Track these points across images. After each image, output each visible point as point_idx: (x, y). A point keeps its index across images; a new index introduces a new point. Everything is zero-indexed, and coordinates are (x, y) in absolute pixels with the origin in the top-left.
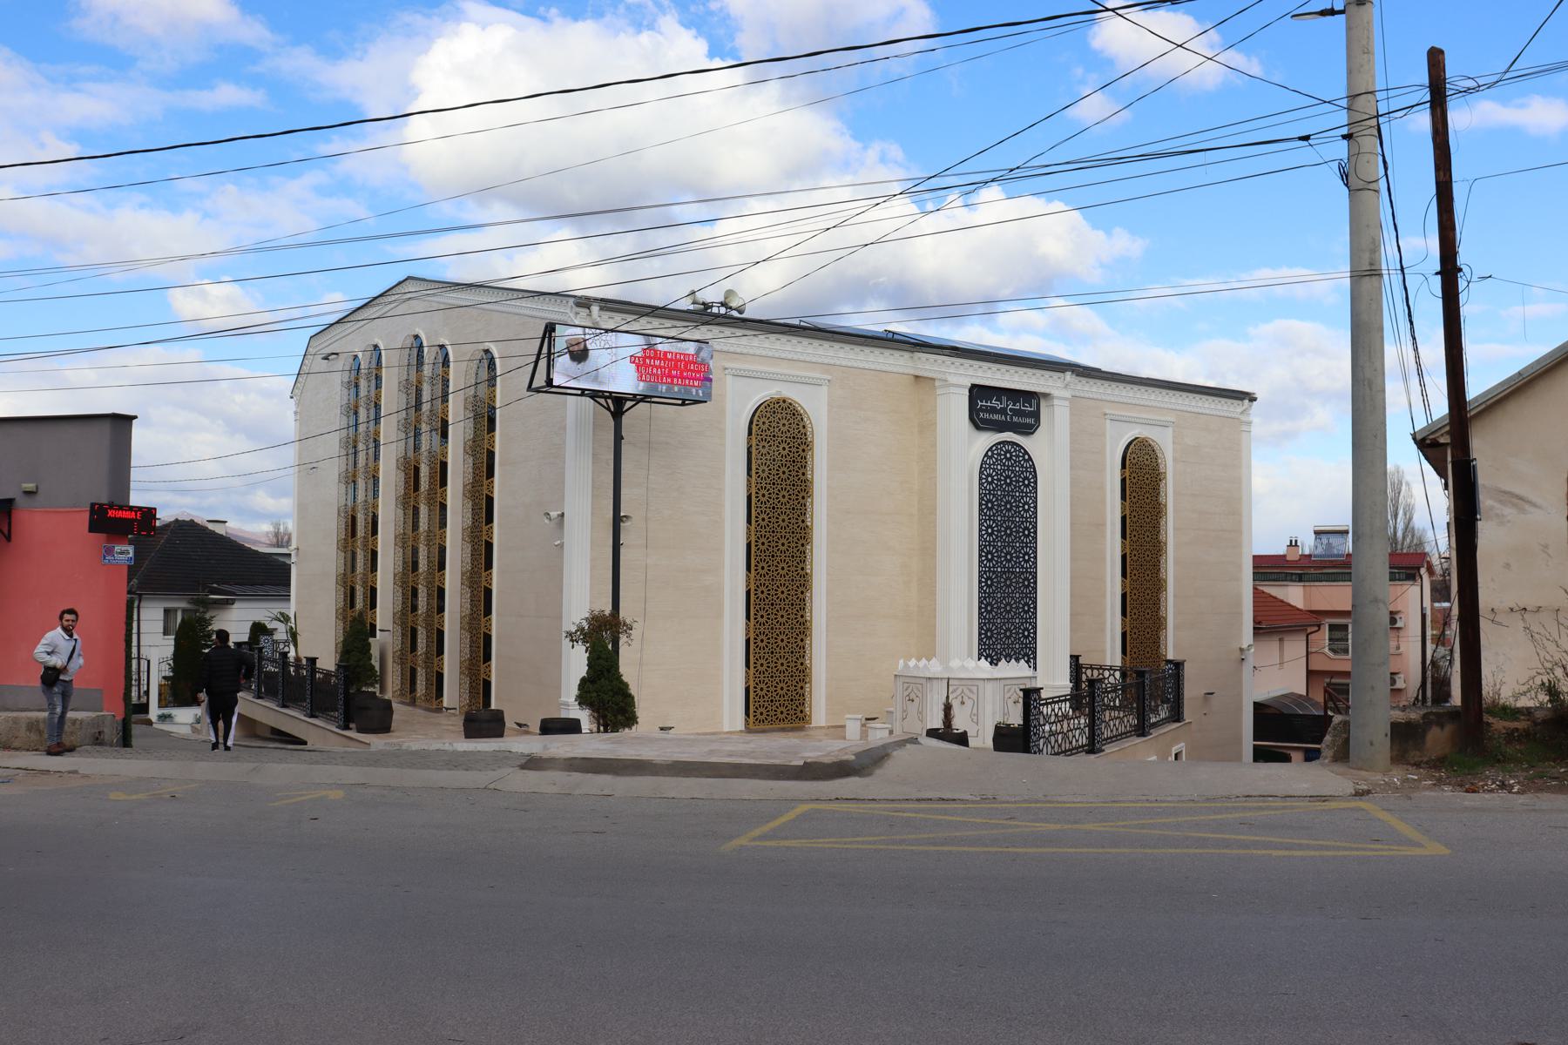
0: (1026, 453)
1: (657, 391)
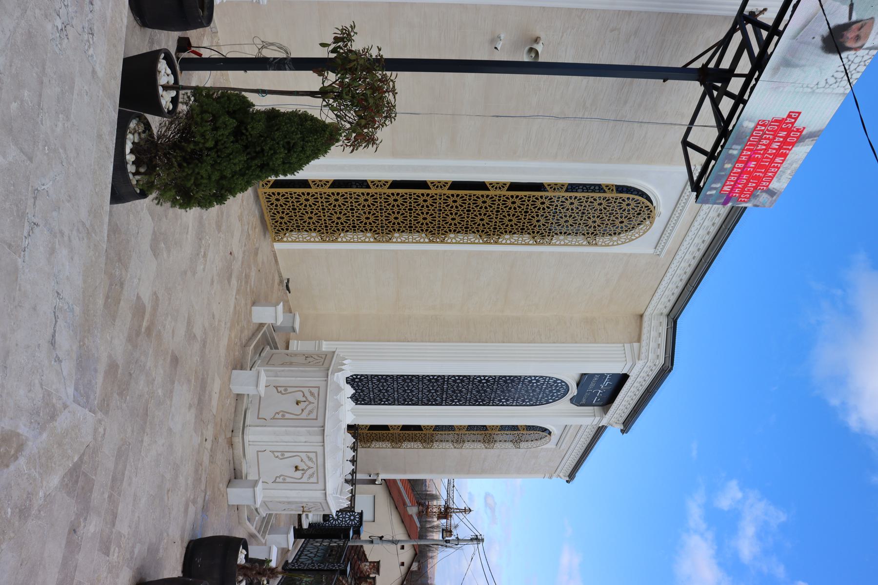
1: (734, 143)
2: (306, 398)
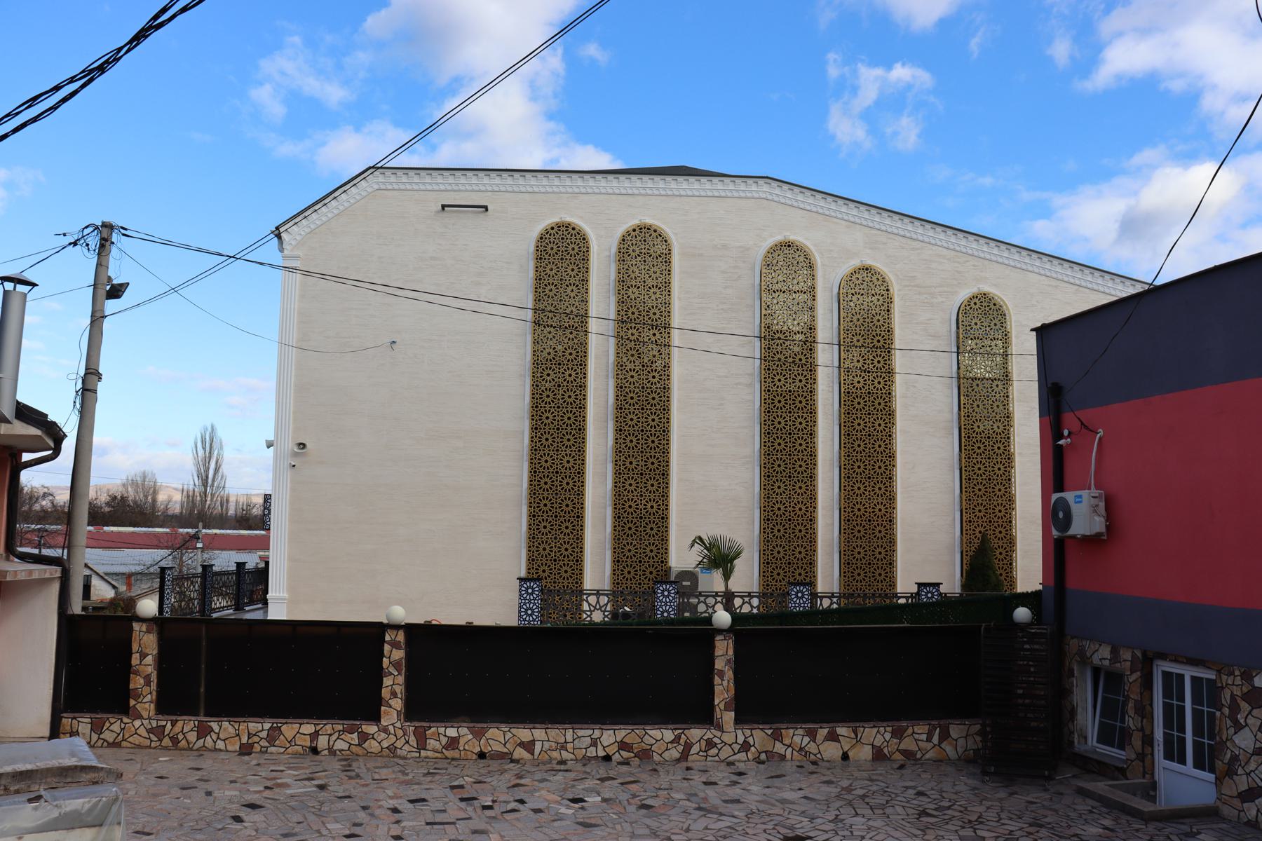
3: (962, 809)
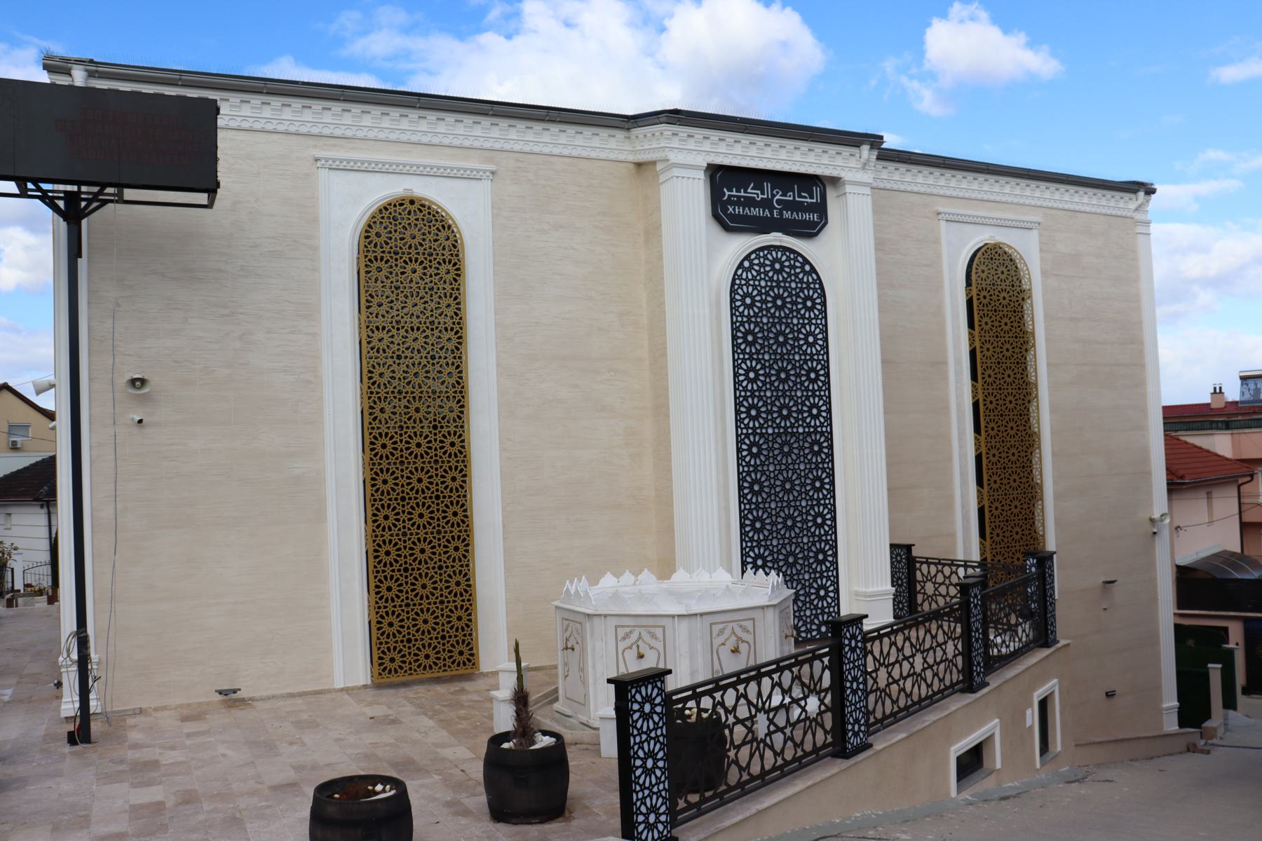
0: (806, 261)
2: (632, 645)
3: (952, 629)
